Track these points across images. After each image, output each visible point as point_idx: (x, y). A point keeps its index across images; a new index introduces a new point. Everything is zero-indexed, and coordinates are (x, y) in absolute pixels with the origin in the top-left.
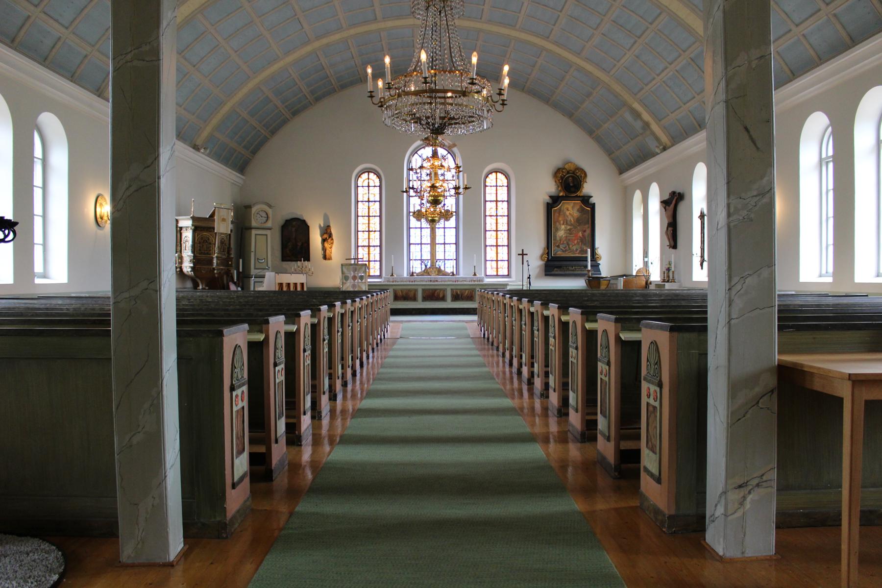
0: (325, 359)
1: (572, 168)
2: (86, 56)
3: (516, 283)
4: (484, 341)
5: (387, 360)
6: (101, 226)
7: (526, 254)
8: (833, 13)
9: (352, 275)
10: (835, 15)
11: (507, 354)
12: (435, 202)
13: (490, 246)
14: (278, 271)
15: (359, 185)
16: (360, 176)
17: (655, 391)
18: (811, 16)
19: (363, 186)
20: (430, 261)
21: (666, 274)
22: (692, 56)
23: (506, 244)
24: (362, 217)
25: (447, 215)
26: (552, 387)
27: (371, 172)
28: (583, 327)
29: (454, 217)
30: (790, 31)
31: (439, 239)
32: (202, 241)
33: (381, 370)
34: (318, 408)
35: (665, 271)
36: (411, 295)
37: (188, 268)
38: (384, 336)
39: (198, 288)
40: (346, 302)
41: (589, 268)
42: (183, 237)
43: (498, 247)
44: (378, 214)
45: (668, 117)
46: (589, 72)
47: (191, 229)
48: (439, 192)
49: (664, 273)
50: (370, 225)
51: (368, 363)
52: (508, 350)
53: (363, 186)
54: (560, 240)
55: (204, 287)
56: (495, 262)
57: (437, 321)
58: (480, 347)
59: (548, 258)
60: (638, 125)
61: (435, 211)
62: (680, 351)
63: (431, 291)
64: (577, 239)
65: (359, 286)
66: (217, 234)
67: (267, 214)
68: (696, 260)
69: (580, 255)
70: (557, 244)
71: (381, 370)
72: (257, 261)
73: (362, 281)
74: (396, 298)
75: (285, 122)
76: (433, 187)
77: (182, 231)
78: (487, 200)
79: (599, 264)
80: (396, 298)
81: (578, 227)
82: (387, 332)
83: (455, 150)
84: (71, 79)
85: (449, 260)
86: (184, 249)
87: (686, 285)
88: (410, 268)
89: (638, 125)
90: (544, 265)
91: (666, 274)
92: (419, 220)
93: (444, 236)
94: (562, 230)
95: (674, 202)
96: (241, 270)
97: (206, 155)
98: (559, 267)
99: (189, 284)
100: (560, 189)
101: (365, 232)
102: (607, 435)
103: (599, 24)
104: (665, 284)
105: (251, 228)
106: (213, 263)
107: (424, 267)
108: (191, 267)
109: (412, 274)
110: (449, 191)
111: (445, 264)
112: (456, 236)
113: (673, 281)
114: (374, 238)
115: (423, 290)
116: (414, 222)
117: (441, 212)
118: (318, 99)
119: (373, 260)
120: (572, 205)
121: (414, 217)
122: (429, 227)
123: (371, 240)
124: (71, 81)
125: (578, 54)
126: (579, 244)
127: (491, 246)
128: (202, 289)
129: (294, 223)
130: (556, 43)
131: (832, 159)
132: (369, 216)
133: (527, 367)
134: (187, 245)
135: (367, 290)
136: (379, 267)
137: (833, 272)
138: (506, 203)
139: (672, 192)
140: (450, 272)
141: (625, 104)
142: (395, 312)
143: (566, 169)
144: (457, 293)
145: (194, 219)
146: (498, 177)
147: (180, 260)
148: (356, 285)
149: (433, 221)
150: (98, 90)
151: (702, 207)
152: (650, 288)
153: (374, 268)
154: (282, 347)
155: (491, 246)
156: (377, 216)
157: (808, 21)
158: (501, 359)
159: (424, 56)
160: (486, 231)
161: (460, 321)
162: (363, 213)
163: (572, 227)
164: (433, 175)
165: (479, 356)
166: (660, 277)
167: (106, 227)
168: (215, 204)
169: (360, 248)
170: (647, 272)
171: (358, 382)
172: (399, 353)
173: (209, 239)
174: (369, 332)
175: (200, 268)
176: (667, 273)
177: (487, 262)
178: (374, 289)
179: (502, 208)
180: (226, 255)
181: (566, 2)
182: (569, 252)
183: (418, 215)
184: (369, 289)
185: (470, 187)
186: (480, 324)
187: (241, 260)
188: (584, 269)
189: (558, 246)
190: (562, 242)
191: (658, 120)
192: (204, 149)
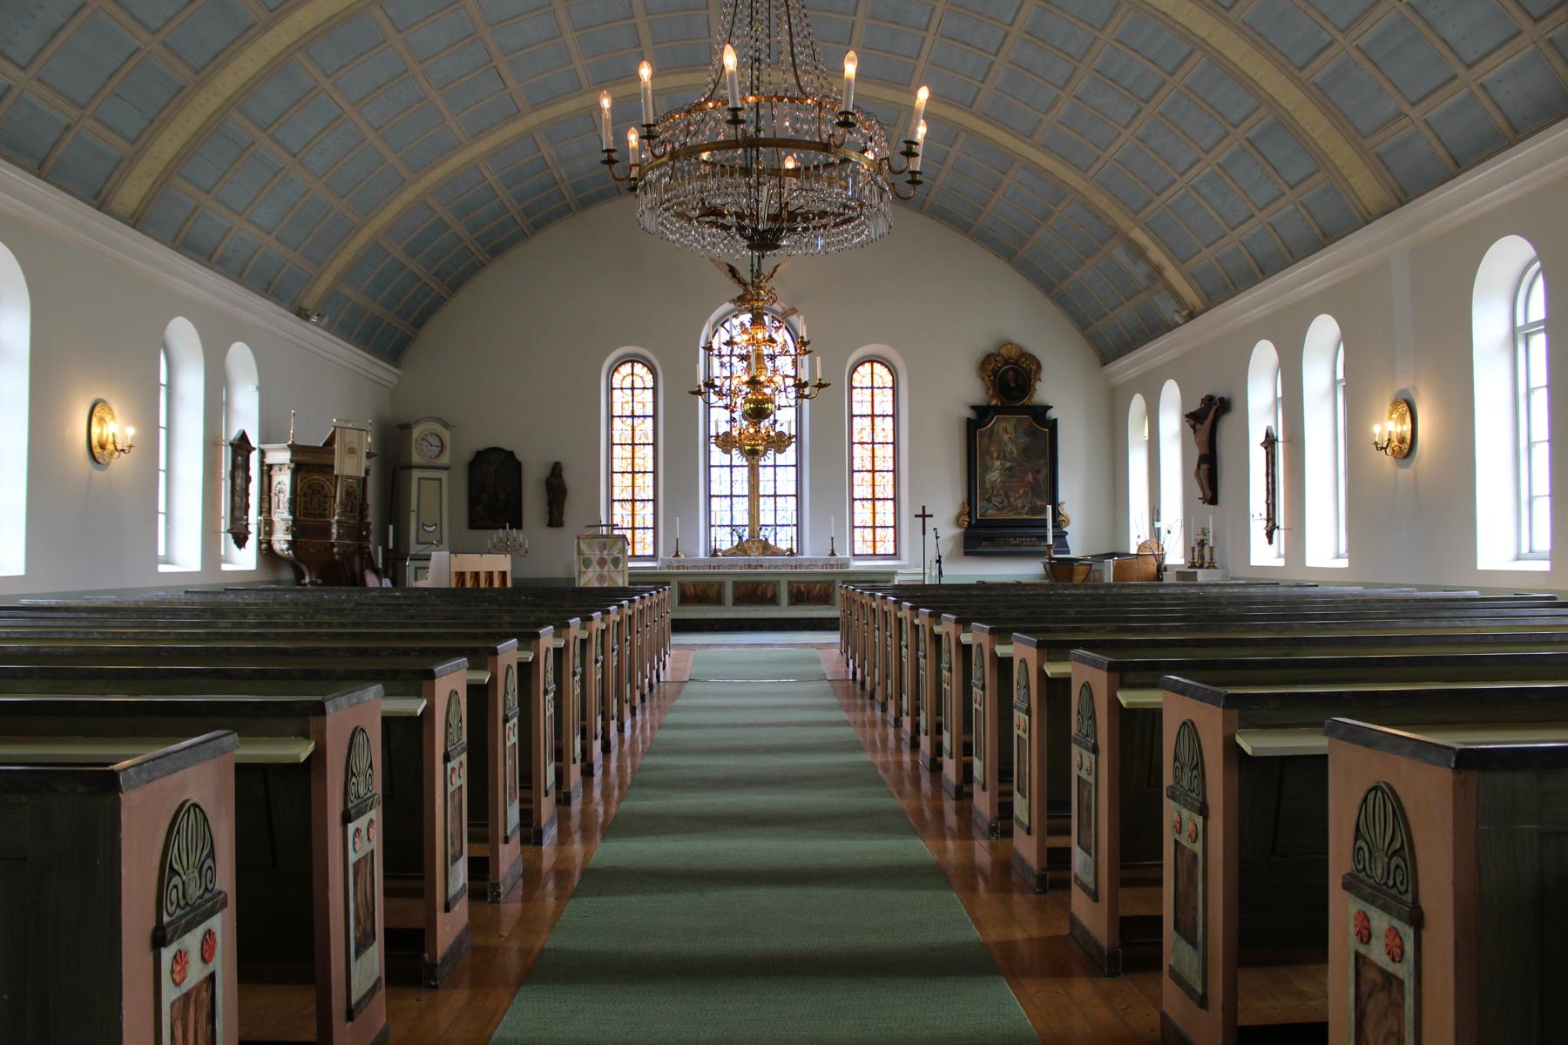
0: (509, 762)
1: (1014, 353)
2: (68, 128)
3: (909, 570)
4: (854, 687)
5: (662, 735)
6: (100, 460)
7: (931, 516)
8: (1547, 36)
9: (597, 557)
10: (1551, 42)
11: (907, 722)
12: (758, 412)
14: (455, 551)
15: (614, 386)
16: (616, 370)
17: (1394, 933)
18: (1499, 46)
19: (622, 389)
20: (747, 528)
21: (1196, 553)
22: (1250, 135)
24: (620, 446)
25: (779, 442)
26: (1020, 823)
27: (638, 362)
28: (1114, 702)
29: (793, 445)
30: (1455, 77)
31: (765, 487)
32: (311, 491)
33: (649, 760)
34: (491, 876)
35: (1196, 546)
36: (713, 593)
37: (282, 542)
38: (658, 677)
39: (302, 582)
40: (568, 623)
41: (1050, 541)
42: (274, 483)
44: (651, 441)
47: (289, 468)
48: (765, 394)
49: (1193, 551)
50: (636, 461)
51: (622, 741)
52: (907, 714)
53: (622, 389)
55: (314, 579)
56: (870, 530)
57: (761, 645)
58: (845, 701)
59: (969, 523)
60: (1140, 271)
61: (757, 432)
62: (1486, 827)
65: (611, 579)
66: (339, 478)
67: (441, 440)
68: (1258, 527)
71: (649, 760)
72: (421, 526)
74: (685, 599)
75: (477, 267)
76: (753, 382)
77: (272, 473)
79: (1066, 533)
80: (685, 599)
81: (1026, 464)
82: (664, 668)
83: (793, 319)
84: (37, 171)
85: (783, 526)
86: (276, 506)
87: (1238, 573)
88: (710, 541)
89: (1140, 271)
91: (1196, 553)
93: (775, 481)
95: (1211, 416)
96: (391, 546)
97: (324, 329)
99: (287, 574)
100: (991, 392)
101: (626, 474)
102: (1200, 991)
103: (1068, 80)
104: (1196, 573)
105: (409, 467)
106: (332, 533)
107: (736, 539)
108: (288, 542)
109: (715, 553)
110: (785, 390)
111: (776, 534)
112: (797, 481)
113: (1212, 566)
115: (736, 584)
116: (717, 456)
117: (769, 435)
118: (537, 226)
119: (642, 526)
120: (1014, 422)
121: (717, 446)
122: (746, 464)
123: (636, 490)
124: (39, 176)
125: (1027, 137)
126: (1028, 496)
127: (863, 499)
128: (312, 583)
130: (986, 117)
131: (1543, 327)
132: (633, 444)
133: (954, 760)
135: (627, 585)
136: (652, 539)
137: (1551, 551)
138: (890, 419)
139: (1207, 396)
140: (785, 549)
141: (1115, 232)
142: (681, 626)
145: (294, 448)
146: (875, 371)
147: (267, 528)
149: (752, 454)
150: (96, 197)
151: (1270, 425)
152: (1165, 581)
153: (643, 541)
154: (371, 766)
155: (863, 499)
156: (649, 444)
157: (1495, 55)
158: (891, 731)
159: (730, 60)
160: (853, 471)
161: (806, 645)
162: (623, 439)
163: (1015, 464)
164: (753, 360)
165: (846, 724)
166: (1185, 557)
167: (110, 467)
168: (335, 420)
169: (616, 505)
170: (1160, 548)
171: (597, 793)
172: (694, 702)
173: (323, 487)
174: (627, 673)
175: (306, 542)
176: (1200, 551)
177: (856, 530)
178: (643, 583)
179: (883, 429)
180: (358, 518)
181: (1022, 4)
182: (1008, 512)
183: (726, 442)
184: (630, 583)
185: (828, 383)
186: (847, 651)
187: (391, 527)
188: (1038, 543)
189: (989, 500)
190: (995, 492)
191: (1180, 261)
192: (318, 315)
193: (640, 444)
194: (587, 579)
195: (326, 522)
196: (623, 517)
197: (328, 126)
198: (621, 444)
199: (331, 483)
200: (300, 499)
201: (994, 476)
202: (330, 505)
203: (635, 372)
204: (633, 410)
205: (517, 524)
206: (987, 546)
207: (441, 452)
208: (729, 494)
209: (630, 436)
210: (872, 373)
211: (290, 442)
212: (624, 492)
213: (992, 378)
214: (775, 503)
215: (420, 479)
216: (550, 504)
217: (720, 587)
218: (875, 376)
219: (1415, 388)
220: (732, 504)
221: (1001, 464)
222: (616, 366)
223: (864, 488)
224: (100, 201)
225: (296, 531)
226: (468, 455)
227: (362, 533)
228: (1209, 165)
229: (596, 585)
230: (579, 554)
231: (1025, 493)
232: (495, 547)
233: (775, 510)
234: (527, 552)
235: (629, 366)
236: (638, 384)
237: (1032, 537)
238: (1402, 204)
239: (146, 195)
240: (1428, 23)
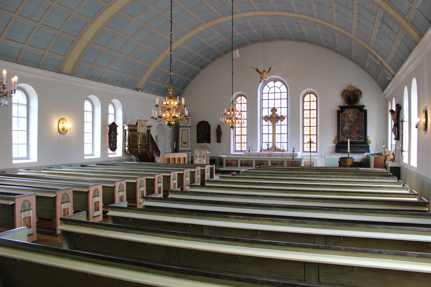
1: (353, 89)
2: (43, 55)
6: (62, 133)
9: (199, 155)
13: (306, 135)
25: (282, 118)
27: (243, 96)
36: (250, 163)
45: (388, 57)
54: (345, 132)
59: (338, 142)
63: (260, 162)
64: (356, 131)
65: (203, 161)
66: (140, 133)
69: (357, 141)
70: (344, 134)
73: (204, 158)
79: (369, 146)
81: (357, 124)
90: (335, 147)
93: (281, 129)
94: (346, 126)
100: (345, 102)
114: (243, 131)
115: (256, 161)
116: (264, 122)
127: (307, 135)
129: (203, 123)
143: (349, 90)
147: (125, 146)
150: (58, 70)
153: (244, 147)
155: (307, 135)
156: (245, 119)
173: (136, 135)
188: (360, 149)
189: (344, 135)
190: (346, 133)
197: (125, 43)
199: (138, 134)
200: (131, 139)
201: (346, 128)
203: (242, 99)
205: (209, 142)
206: (343, 150)
207: (188, 122)
210: (310, 97)
211: (128, 124)
213: (345, 97)
214: (281, 136)
215: (182, 130)
216: (217, 136)
221: (348, 124)
223: (307, 131)
224: (59, 71)
225: (129, 147)
227: (148, 147)
234: (210, 150)
235: (240, 97)
236: (243, 102)
237: (358, 147)
239: (73, 67)
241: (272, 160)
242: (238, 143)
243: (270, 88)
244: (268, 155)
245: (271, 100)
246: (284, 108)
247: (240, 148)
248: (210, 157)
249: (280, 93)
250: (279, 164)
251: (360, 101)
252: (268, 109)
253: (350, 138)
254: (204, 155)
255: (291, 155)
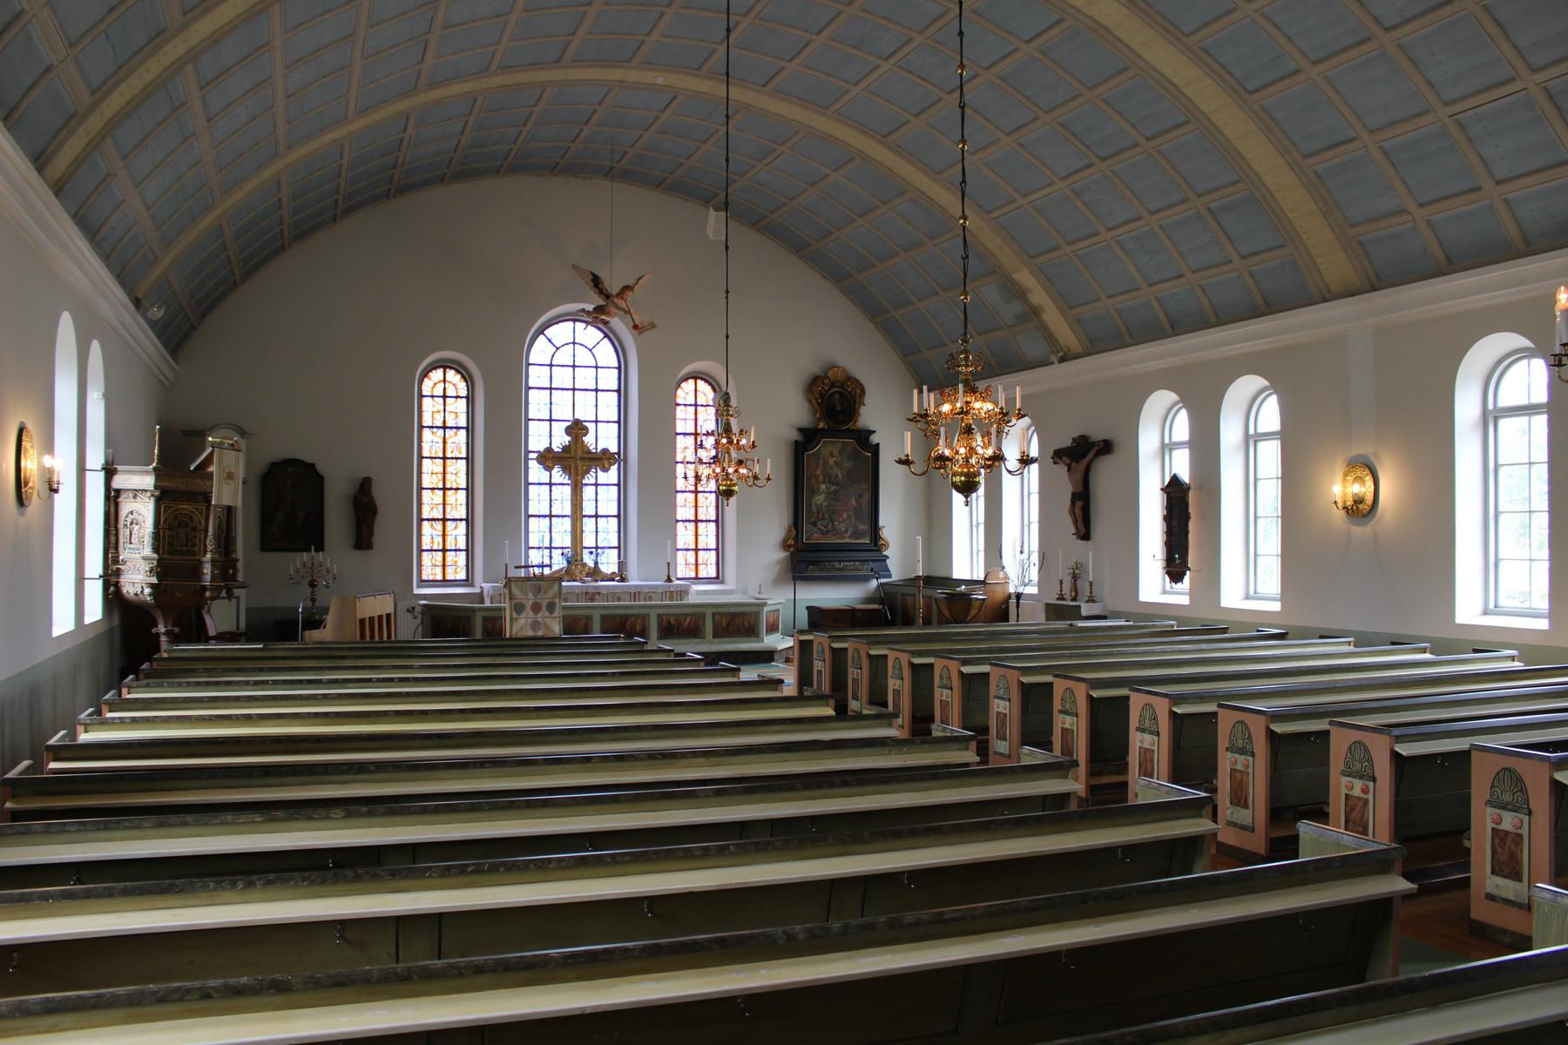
1: (840, 376)
9: (531, 602)
13: (683, 521)
19: (432, 396)
23: (714, 518)
24: (429, 460)
25: (603, 459)
27: (451, 368)
30: (1479, 189)
31: (588, 508)
32: (176, 524)
43: (693, 518)
46: (941, 206)
50: (448, 476)
53: (432, 396)
56: (693, 553)
65: (547, 626)
70: (813, 520)
77: (120, 499)
78: (424, 393)
79: (887, 557)
92: (549, 469)
93: (596, 500)
98: (816, 563)
100: (818, 415)
101: (436, 491)
108: (152, 586)
114: (453, 502)
115: (603, 617)
116: (536, 472)
119: (453, 548)
120: (839, 446)
122: (567, 481)
123: (448, 508)
127: (686, 521)
132: (444, 458)
134: (135, 532)
144: (669, 622)
146: (698, 389)
148: (539, 623)
153: (455, 564)
155: (686, 521)
156: (462, 458)
162: (433, 452)
173: (191, 518)
182: (833, 535)
188: (861, 567)
189: (814, 524)
190: (820, 516)
193: (452, 458)
194: (520, 625)
195: (195, 560)
196: (432, 538)
198: (431, 458)
200: (164, 532)
201: (820, 499)
202: (200, 540)
203: (447, 379)
204: (444, 421)
205: (320, 548)
208: (548, 514)
209: (442, 449)
210: (696, 390)
212: (434, 509)
213: (820, 401)
214: (597, 524)
217: (588, 621)
218: (699, 394)
219: (1375, 454)
220: (551, 525)
222: (462, 371)
226: (260, 468)
228: (1149, 224)
229: (530, 633)
230: (511, 599)
231: (849, 517)
232: (298, 572)
233: (597, 532)
235: (440, 371)
238: (1374, 289)
240: (1470, 139)
241: (661, 611)
242: (432, 550)
243: (558, 346)
244: (587, 593)
245: (560, 391)
246: (608, 422)
247: (439, 571)
248: (248, 610)
249: (594, 369)
250: (687, 623)
251: (859, 414)
252: (548, 423)
253: (831, 531)
254: (550, 600)
255: (668, 594)
